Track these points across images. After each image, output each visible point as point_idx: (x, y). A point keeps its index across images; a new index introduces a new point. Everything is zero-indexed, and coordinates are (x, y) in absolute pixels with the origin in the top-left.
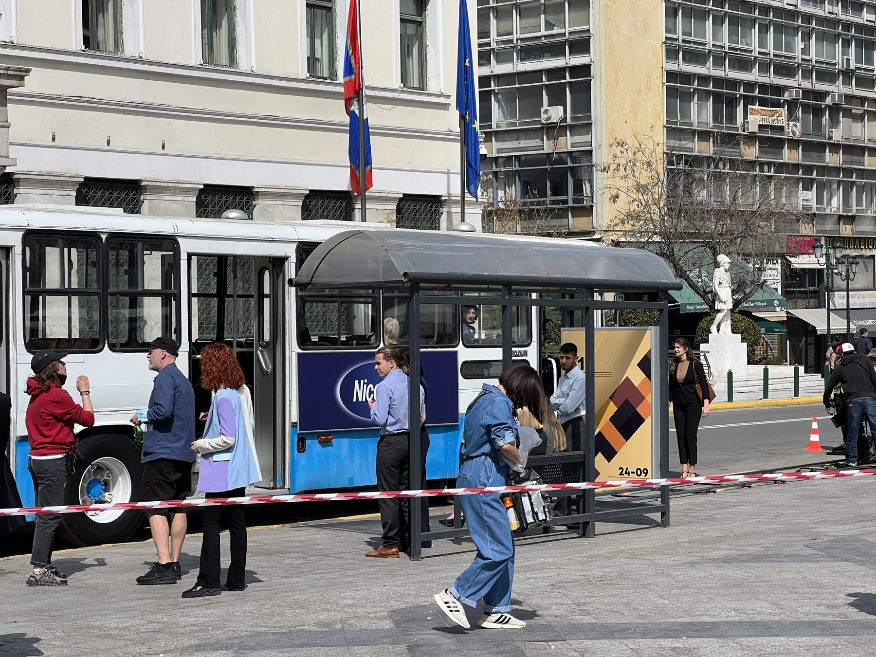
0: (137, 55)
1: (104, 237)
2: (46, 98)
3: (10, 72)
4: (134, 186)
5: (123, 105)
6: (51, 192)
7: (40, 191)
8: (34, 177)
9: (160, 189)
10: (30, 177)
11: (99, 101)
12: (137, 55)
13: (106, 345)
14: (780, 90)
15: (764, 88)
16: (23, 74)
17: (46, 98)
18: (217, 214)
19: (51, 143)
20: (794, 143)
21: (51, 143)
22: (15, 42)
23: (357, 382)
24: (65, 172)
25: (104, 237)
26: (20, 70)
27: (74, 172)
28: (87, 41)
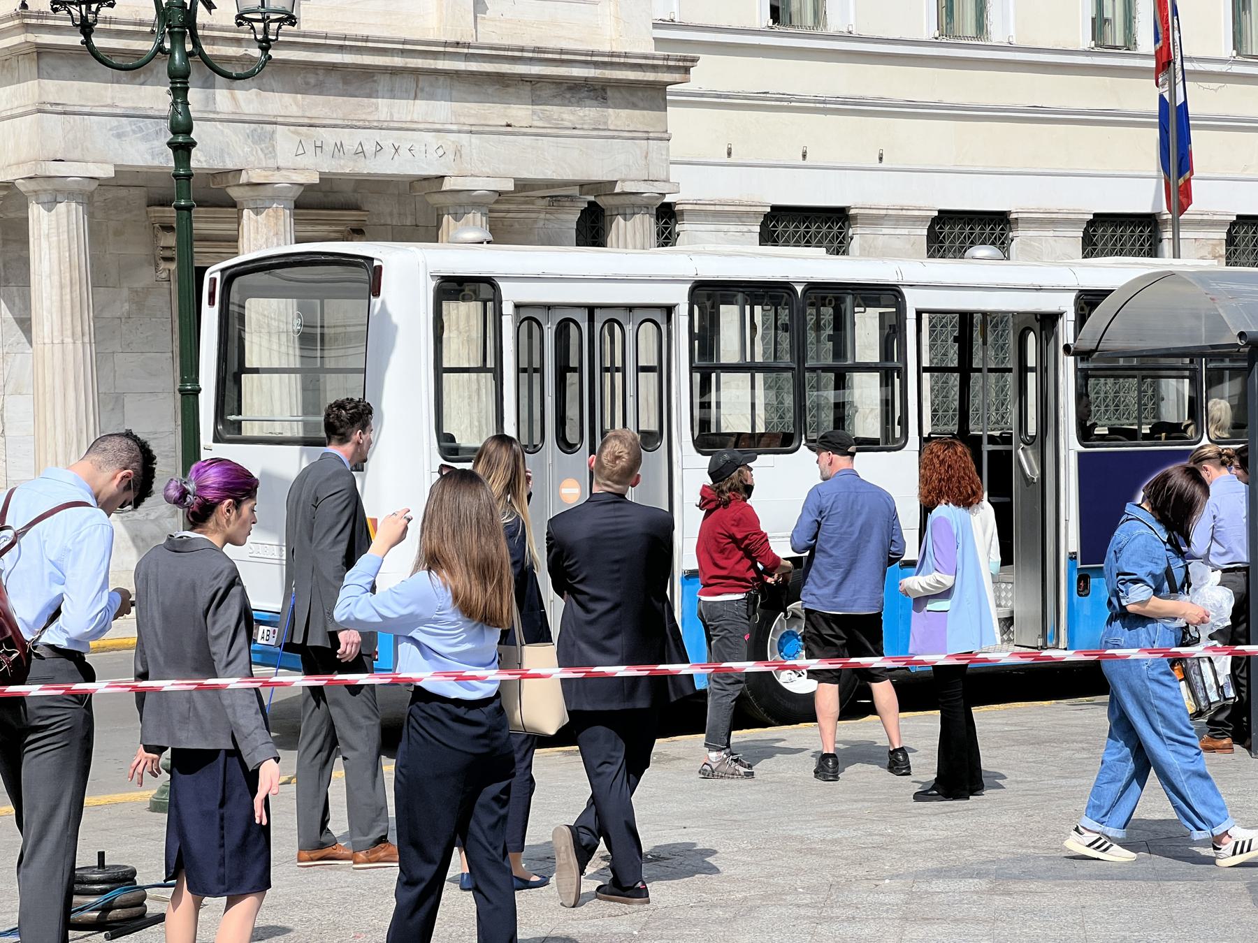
0: (845, 30)
1: (799, 289)
2: (719, 96)
6: (725, 228)
9: (876, 220)
10: (697, 207)
11: (790, 98)
12: (845, 30)
16: (689, 64)
17: (719, 96)
19: (726, 159)
21: (726, 159)
24: (745, 199)
25: (799, 289)
27: (757, 199)
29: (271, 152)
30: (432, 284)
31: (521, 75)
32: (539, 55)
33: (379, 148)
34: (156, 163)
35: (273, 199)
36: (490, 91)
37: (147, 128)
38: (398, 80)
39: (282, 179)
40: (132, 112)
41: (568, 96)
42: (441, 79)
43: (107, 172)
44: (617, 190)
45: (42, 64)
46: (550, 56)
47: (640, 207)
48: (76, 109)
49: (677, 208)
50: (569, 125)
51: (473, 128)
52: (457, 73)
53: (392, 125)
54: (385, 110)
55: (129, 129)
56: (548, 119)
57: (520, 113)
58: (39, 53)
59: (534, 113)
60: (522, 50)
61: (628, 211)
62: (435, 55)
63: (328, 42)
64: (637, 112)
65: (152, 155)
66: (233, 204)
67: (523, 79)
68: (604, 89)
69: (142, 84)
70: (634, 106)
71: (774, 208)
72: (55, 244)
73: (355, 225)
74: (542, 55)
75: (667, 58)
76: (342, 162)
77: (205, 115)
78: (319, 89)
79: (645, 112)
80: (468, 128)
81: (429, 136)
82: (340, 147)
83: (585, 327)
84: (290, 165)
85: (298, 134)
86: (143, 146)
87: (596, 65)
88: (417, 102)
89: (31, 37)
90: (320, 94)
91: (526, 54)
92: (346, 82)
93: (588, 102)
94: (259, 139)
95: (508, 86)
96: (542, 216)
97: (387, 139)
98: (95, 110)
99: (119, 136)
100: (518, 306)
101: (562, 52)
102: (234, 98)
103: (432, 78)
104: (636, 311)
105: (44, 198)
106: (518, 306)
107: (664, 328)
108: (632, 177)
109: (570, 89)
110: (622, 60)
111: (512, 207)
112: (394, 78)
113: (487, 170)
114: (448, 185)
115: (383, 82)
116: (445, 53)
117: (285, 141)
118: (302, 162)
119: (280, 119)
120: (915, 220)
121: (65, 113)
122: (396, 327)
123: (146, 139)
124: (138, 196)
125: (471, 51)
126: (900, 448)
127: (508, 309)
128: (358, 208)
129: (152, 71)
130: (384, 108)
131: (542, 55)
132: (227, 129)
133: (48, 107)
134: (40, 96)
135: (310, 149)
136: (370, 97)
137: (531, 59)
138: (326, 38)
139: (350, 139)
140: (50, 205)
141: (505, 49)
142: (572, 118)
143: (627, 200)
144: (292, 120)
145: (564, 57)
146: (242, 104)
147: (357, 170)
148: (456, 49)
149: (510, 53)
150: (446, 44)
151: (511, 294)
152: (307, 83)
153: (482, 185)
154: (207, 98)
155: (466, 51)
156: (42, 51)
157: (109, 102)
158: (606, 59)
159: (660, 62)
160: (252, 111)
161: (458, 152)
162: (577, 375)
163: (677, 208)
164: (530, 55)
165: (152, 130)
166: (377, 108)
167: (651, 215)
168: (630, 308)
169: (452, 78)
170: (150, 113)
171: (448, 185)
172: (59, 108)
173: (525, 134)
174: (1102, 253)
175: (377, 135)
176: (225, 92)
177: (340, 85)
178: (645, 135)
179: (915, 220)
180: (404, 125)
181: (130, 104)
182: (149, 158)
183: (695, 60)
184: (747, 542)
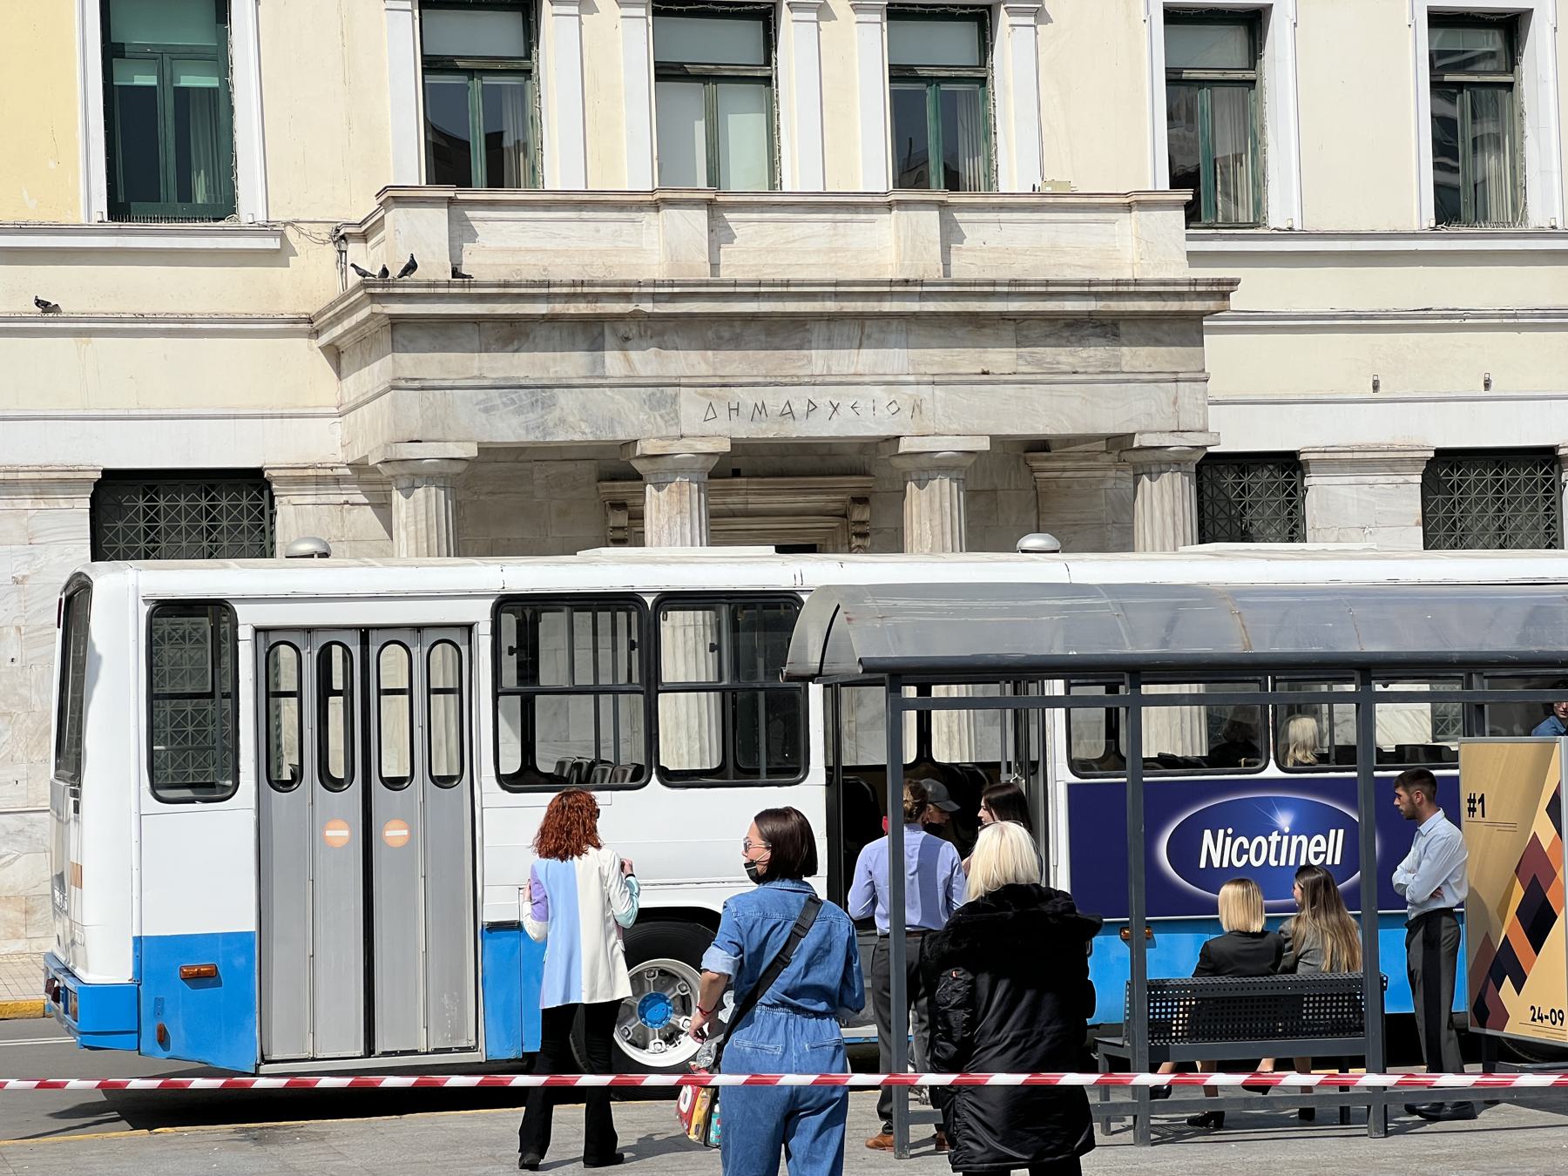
0: (1547, 225)
1: (649, 600)
2: (1359, 317)
3: (1199, 289)
4: (1546, 457)
5: (1515, 316)
6: (1371, 479)
7: (1352, 479)
8: (1336, 456)
10: (1327, 456)
11: (1465, 314)
12: (1547, 225)
13: (654, 776)
16: (1225, 288)
17: (1359, 317)
18: (1007, 544)
19: (1370, 394)
21: (1370, 394)
22: (1297, 227)
23: (1207, 833)
24: (1399, 442)
25: (649, 600)
26: (1219, 282)
27: (1417, 441)
28: (1451, 207)
30: (145, 609)
31: (1000, 313)
32: (1016, 288)
33: (812, 407)
34: (531, 438)
35: (676, 471)
36: (960, 333)
37: (521, 399)
38: (836, 329)
39: (682, 449)
40: (502, 383)
41: (1066, 334)
42: (895, 323)
43: (471, 451)
44: (1136, 445)
45: (397, 337)
46: (1032, 289)
47: (1169, 464)
48: (436, 383)
49: (1302, 457)
50: (1068, 369)
51: (936, 379)
52: (915, 316)
53: (828, 379)
54: (820, 363)
55: (498, 402)
56: (1039, 363)
57: (1001, 358)
58: (393, 325)
59: (1019, 357)
60: (994, 284)
61: (1154, 469)
62: (880, 296)
63: (738, 289)
64: (1163, 350)
65: (527, 429)
66: (639, 477)
67: (1004, 317)
68: (1115, 324)
69: (516, 351)
70: (1158, 342)
71: (1438, 452)
72: (412, 534)
73: (858, 493)
74: (1022, 289)
75: (1195, 283)
76: (764, 426)
77: (591, 381)
78: (736, 343)
79: (1173, 349)
80: (931, 379)
81: (878, 391)
82: (761, 409)
83: (356, 651)
84: (697, 432)
85: (707, 395)
86: (515, 421)
87: (1098, 296)
88: (863, 351)
89: (377, 308)
90: (737, 348)
91: (998, 289)
92: (769, 333)
93: (1093, 340)
94: (655, 405)
95: (984, 326)
96: (1112, 473)
97: (823, 397)
98: (457, 384)
99: (487, 410)
100: (257, 630)
101: (1048, 283)
102: (628, 360)
103: (882, 323)
104: (425, 632)
105: (404, 483)
106: (257, 630)
107: (464, 649)
108: (1155, 428)
109: (1068, 325)
110: (1132, 289)
111: (1069, 464)
112: (832, 325)
113: (955, 427)
114: (905, 446)
115: (819, 330)
116: (891, 293)
117: (691, 407)
118: (710, 428)
119: (683, 381)
121: (422, 389)
122: (100, 658)
123: (519, 411)
124: (587, 470)
125: (925, 289)
126: (797, 783)
127: (245, 633)
128: (865, 473)
129: (528, 335)
130: (819, 360)
131: (1022, 289)
132: (618, 395)
133: (403, 384)
134: (394, 371)
135: (723, 412)
136: (800, 348)
137: (1008, 294)
138: (735, 285)
139: (775, 399)
140: (408, 492)
141: (970, 285)
142: (1071, 360)
143: (1150, 455)
144: (700, 381)
145: (1051, 289)
146: (638, 366)
147: (783, 434)
148: (905, 287)
149: (978, 289)
150: (891, 283)
151: (248, 618)
152: (720, 338)
153: (946, 445)
154: (594, 363)
155: (919, 289)
156: (396, 322)
157: (476, 373)
158: (1110, 289)
159: (1186, 289)
160: (649, 373)
161: (917, 408)
162: (406, 697)
163: (1302, 457)
164: (1006, 289)
165: (527, 402)
166: (810, 362)
167: (1184, 473)
168: (419, 628)
169: (908, 321)
170: (523, 382)
172: (416, 384)
173: (1006, 382)
174: (1215, 539)
175: (809, 392)
176: (617, 353)
177: (763, 338)
178: (1173, 376)
180: (844, 379)
181: (501, 374)
182: (523, 432)
183: (1234, 283)
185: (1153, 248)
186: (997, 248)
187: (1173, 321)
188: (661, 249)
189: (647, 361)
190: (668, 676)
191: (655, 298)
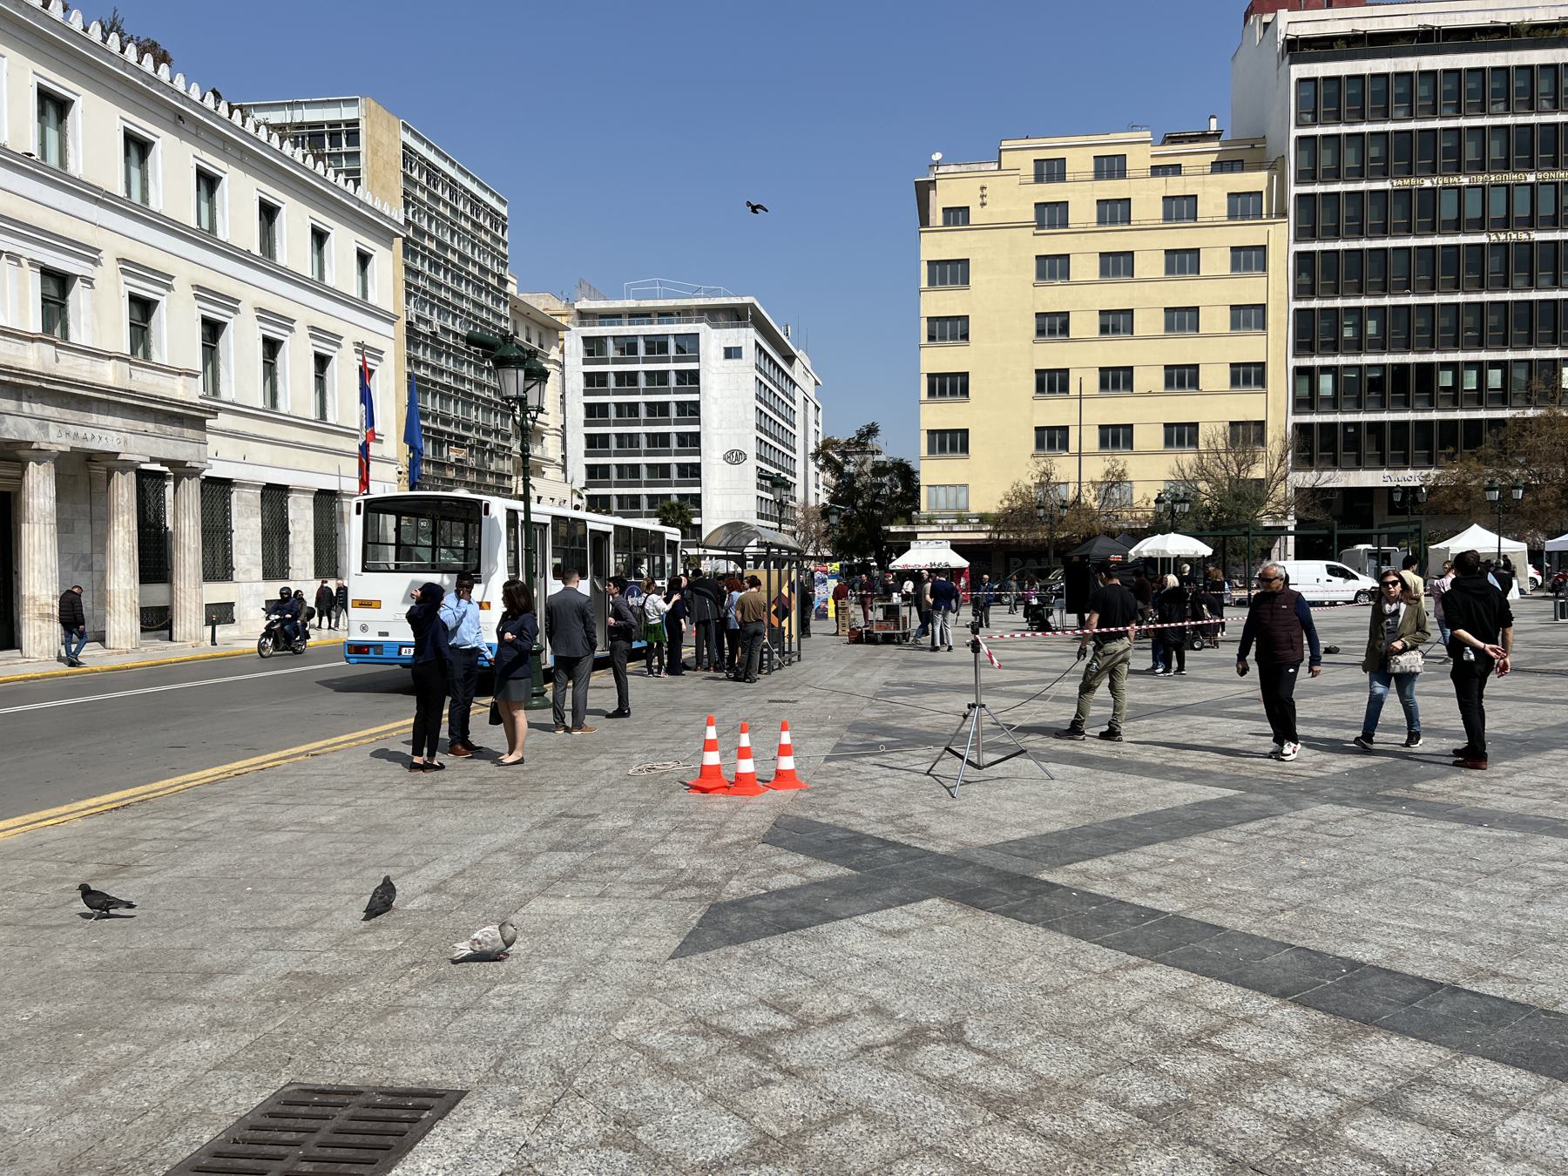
9: (243, 485)
14: (464, 438)
15: (457, 437)
20: (472, 470)
22: (1359, 733)
29: (47, 435)
39: (54, 448)
57: (150, 426)
82: (76, 434)
97: (97, 432)
114: (121, 457)
115: (95, 405)
117: (53, 430)
118: (60, 440)
120: (256, 487)
130: (95, 418)
139: (82, 431)
171: (121, 457)
179: (256, 487)
184: (1175, 664)
185: (188, 391)
186: (145, 382)
187: (190, 419)
188: (109, 374)
189: (38, 409)
190: (591, 704)
191: (47, 381)
